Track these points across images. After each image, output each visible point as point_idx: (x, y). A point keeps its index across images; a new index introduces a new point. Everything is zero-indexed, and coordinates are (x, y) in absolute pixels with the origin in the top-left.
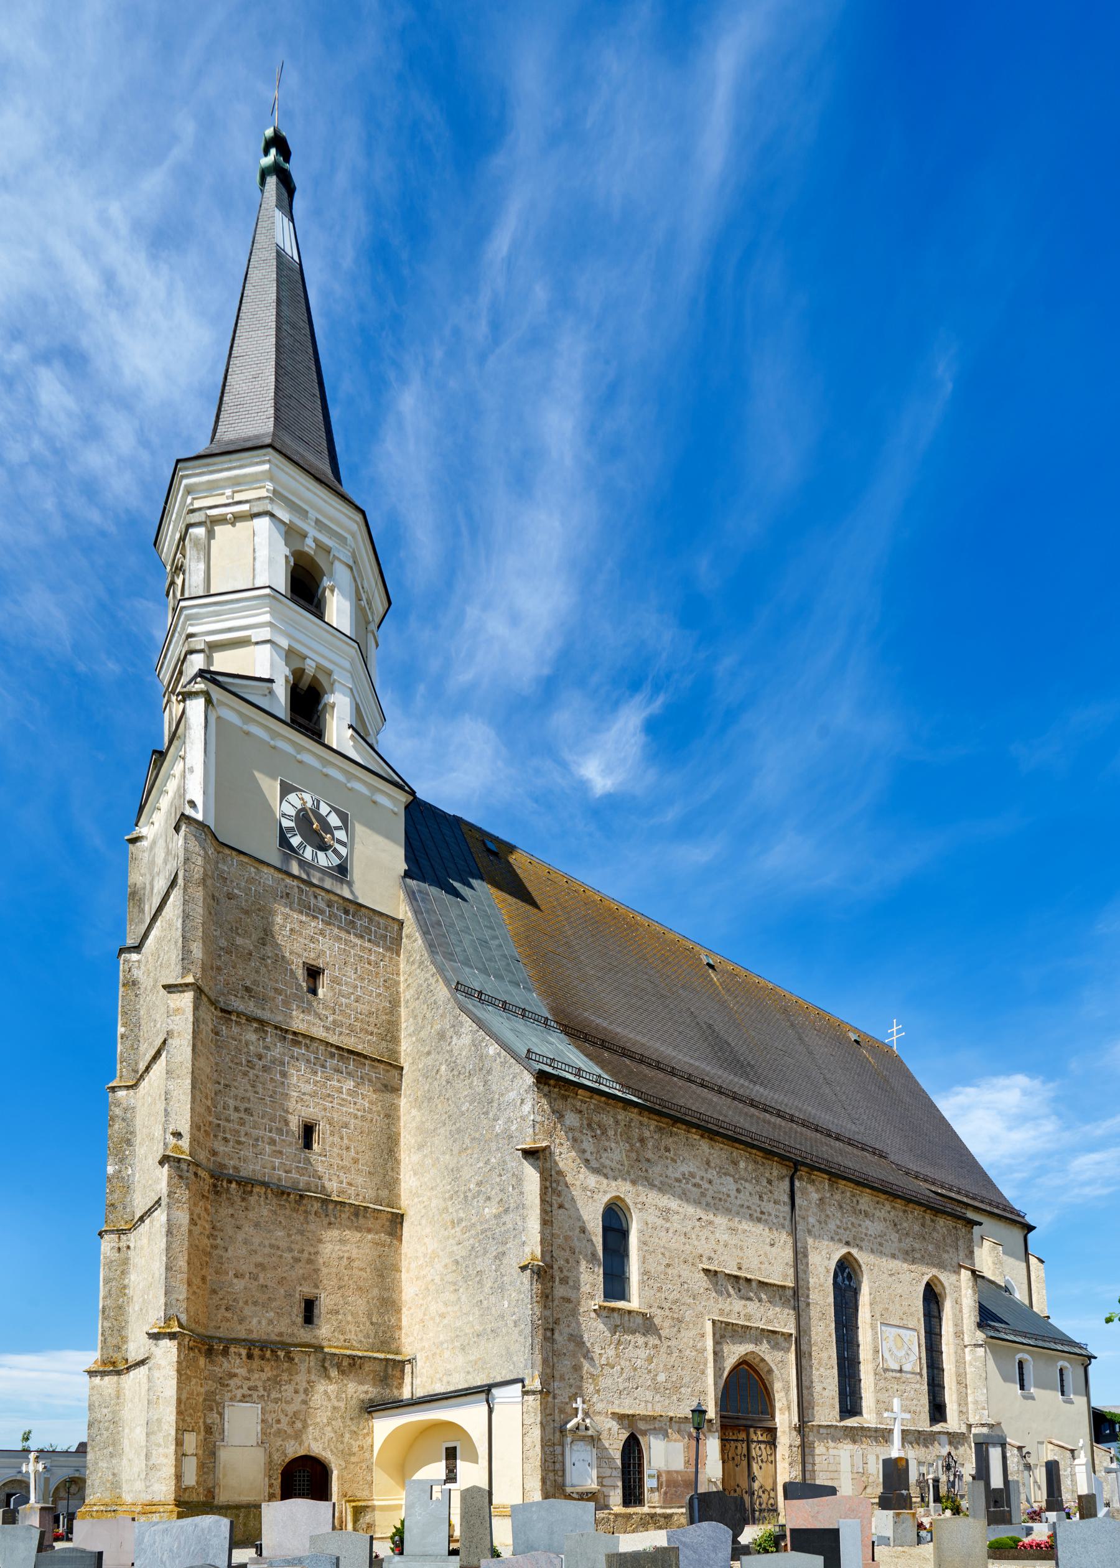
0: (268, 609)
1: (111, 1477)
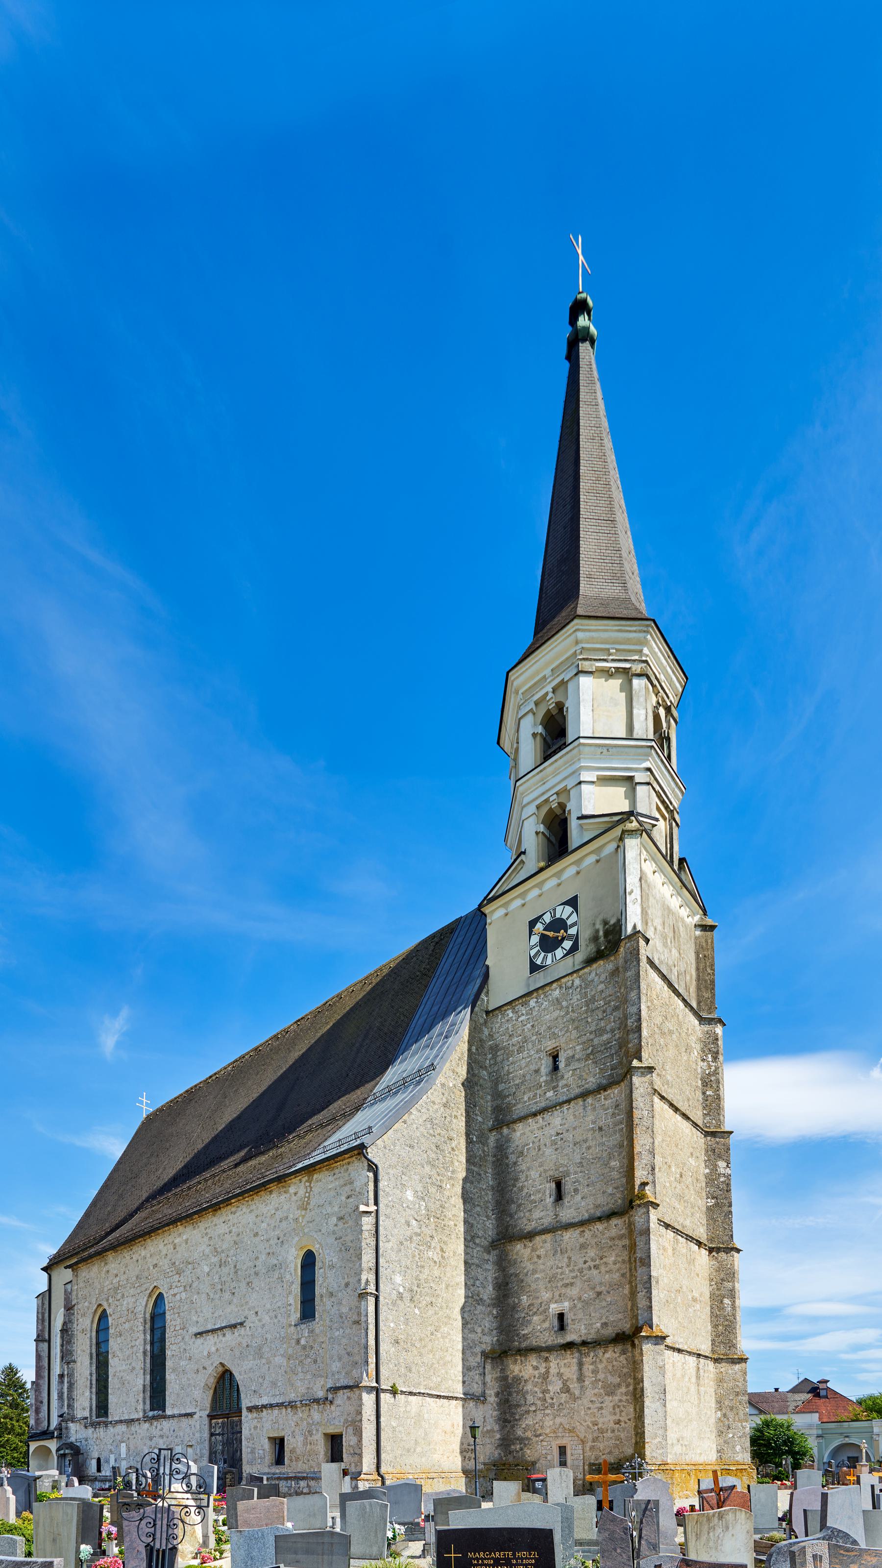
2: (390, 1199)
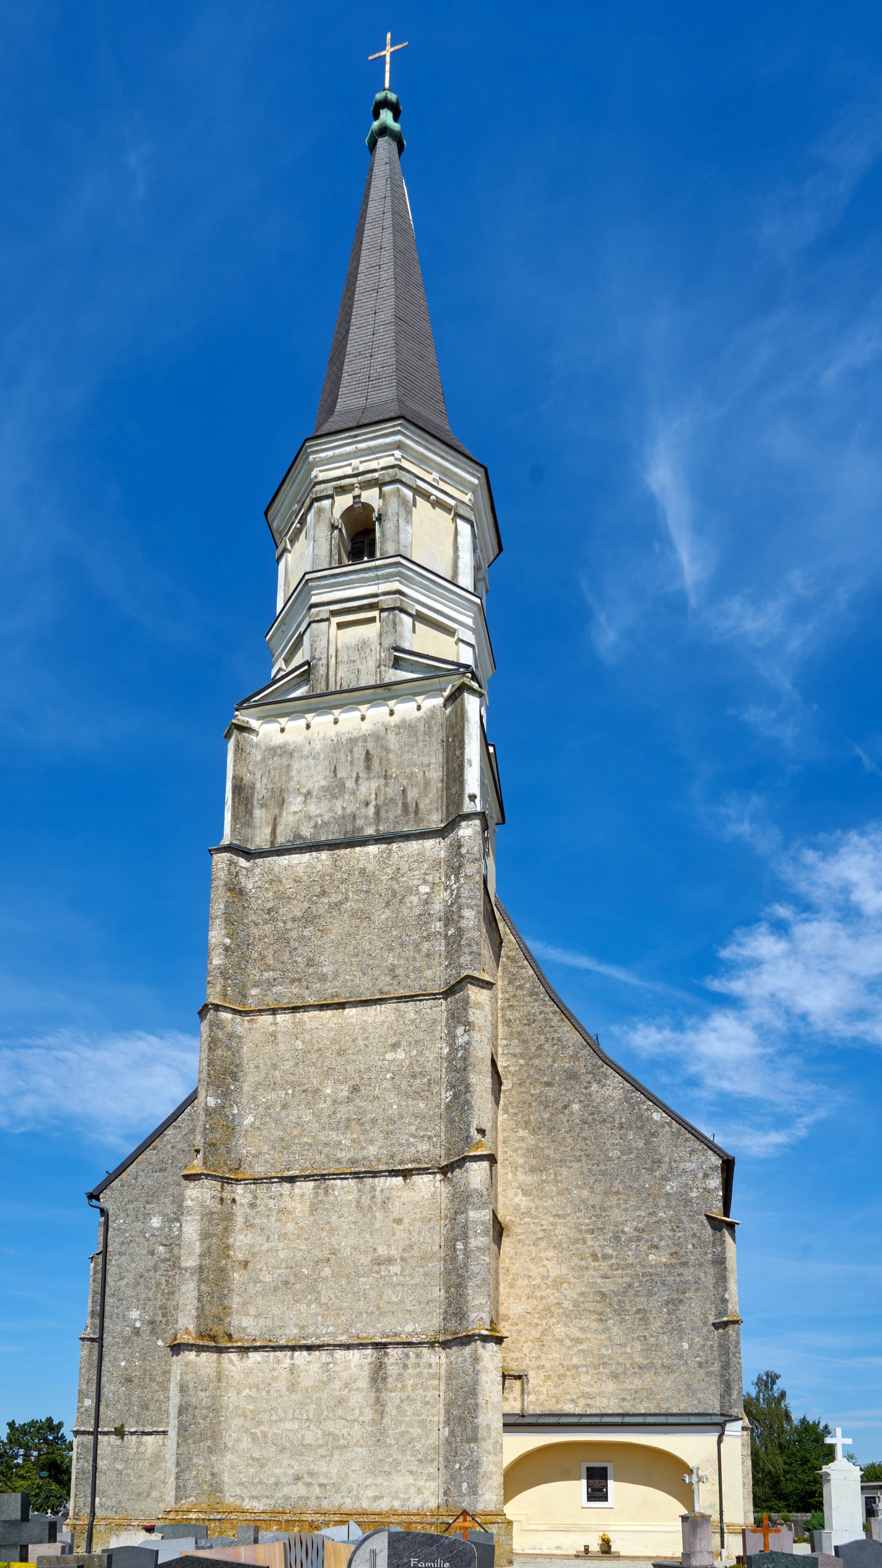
0: (473, 615)
1: (209, 1478)
2: (127, 1235)
